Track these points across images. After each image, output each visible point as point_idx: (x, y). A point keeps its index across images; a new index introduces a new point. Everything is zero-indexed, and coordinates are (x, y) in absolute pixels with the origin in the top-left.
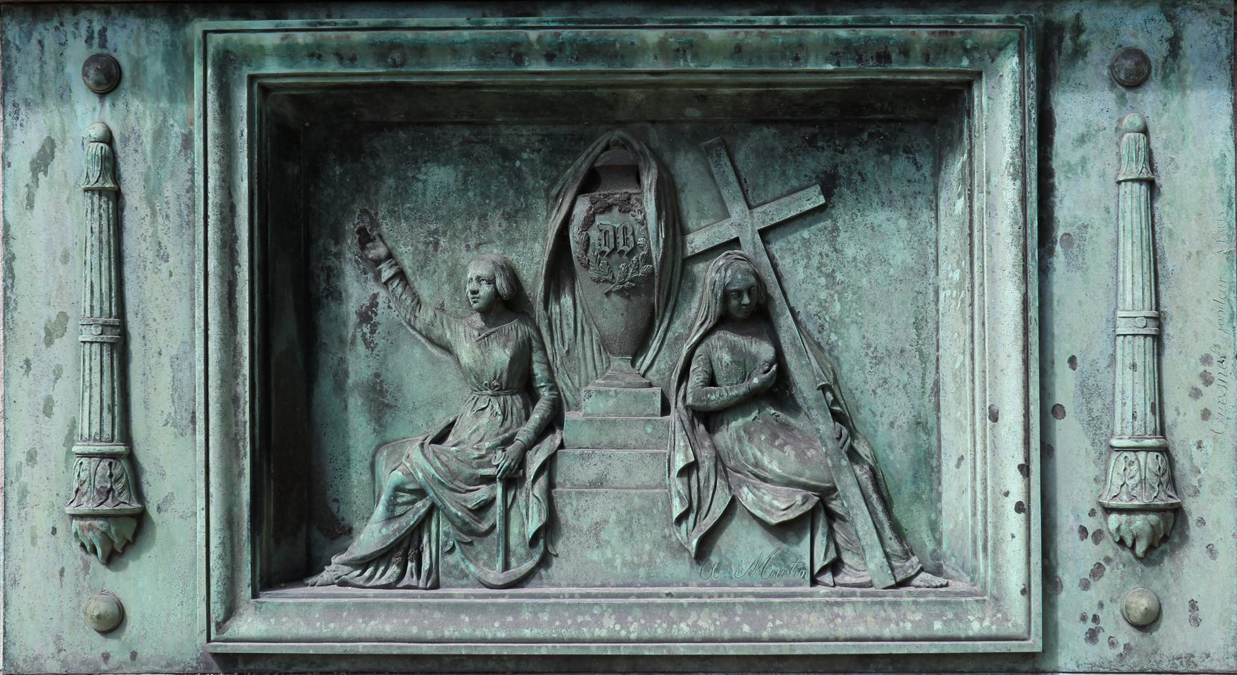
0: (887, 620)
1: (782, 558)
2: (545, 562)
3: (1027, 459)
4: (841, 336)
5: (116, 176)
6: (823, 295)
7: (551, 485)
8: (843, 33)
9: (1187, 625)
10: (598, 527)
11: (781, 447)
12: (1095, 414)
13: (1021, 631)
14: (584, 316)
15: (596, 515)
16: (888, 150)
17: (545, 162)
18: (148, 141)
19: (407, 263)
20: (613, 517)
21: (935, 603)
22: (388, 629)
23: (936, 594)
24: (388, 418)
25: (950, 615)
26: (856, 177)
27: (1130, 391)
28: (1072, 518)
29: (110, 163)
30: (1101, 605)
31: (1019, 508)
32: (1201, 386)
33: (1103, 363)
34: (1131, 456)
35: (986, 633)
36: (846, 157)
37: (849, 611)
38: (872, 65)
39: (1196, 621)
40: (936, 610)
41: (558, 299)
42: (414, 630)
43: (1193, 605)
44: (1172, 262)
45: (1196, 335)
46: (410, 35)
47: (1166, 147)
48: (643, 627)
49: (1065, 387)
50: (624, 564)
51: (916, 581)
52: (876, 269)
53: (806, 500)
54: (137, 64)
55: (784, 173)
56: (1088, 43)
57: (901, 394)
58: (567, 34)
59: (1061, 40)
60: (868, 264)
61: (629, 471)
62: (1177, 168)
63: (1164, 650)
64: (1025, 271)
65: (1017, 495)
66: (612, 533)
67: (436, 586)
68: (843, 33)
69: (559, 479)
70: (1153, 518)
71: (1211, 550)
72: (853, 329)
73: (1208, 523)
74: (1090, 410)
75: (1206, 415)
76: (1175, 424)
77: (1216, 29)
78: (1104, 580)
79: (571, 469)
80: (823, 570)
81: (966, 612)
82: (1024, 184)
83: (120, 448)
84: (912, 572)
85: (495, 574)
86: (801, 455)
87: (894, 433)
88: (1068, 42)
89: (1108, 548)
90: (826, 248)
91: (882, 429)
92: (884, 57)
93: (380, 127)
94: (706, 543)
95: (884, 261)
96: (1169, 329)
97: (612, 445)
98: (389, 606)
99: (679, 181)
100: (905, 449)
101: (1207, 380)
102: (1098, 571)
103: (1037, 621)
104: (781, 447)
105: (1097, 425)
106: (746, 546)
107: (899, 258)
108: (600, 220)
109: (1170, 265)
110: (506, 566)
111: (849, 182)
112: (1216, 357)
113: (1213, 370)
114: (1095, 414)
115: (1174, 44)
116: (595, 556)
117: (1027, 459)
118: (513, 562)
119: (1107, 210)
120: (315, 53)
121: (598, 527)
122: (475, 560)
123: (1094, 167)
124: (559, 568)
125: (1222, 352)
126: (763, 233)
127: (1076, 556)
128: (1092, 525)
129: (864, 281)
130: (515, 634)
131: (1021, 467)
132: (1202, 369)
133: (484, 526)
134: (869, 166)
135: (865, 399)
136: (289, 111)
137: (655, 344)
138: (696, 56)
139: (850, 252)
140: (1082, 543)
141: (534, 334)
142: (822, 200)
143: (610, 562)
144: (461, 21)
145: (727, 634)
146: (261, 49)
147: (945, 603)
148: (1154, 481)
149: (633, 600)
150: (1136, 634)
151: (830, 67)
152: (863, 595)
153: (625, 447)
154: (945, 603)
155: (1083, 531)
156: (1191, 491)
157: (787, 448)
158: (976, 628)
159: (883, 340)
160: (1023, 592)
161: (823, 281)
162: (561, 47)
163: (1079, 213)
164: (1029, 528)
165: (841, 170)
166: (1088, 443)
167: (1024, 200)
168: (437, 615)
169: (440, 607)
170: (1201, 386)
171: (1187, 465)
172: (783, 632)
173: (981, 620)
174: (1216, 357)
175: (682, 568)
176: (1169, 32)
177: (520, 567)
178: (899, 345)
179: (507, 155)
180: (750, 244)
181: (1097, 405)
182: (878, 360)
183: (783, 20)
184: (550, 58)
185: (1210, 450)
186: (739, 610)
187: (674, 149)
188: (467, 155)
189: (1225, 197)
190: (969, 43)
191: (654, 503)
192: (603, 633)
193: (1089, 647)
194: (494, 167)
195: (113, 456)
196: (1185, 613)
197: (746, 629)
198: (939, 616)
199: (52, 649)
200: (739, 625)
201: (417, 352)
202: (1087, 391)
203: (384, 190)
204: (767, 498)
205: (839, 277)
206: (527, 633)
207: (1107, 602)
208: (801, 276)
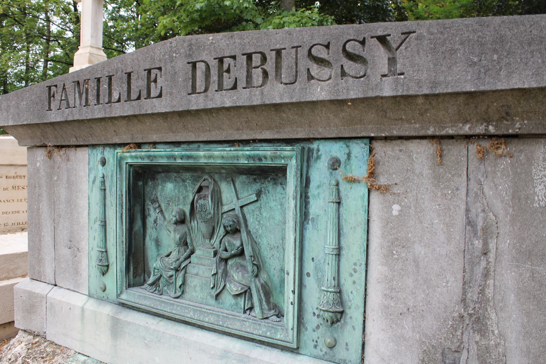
0: (256, 329)
1: (237, 304)
2: (183, 293)
3: (294, 289)
4: (261, 240)
5: (105, 186)
6: (257, 227)
7: (186, 272)
8: (248, 153)
9: (344, 350)
10: (195, 286)
11: (238, 273)
12: (319, 277)
13: (291, 340)
14: (198, 227)
15: (195, 283)
16: (275, 184)
17: (192, 183)
18: (110, 177)
19: (163, 208)
20: (198, 285)
21: (270, 327)
22: (148, 304)
23: (272, 324)
24: (159, 248)
25: (273, 331)
26: (267, 192)
27: (329, 272)
28: (311, 309)
29: (103, 182)
30: (318, 338)
31: (292, 303)
32: (353, 273)
33: (322, 261)
34: (326, 293)
35: (281, 339)
36: (264, 185)
37: (247, 324)
38: (257, 162)
39: (347, 349)
40: (270, 329)
41: (194, 221)
42: (152, 305)
43: (347, 344)
44: (346, 229)
45: (352, 255)
46: (152, 153)
47: (345, 191)
48: (198, 316)
49: (309, 267)
50: (201, 298)
51: (270, 318)
52: (271, 220)
53: (242, 289)
54: (108, 159)
55: (248, 189)
56: (321, 155)
57: (277, 260)
58: (183, 153)
59: (313, 154)
60: (269, 219)
61: (203, 272)
62: (348, 198)
63: (337, 356)
64: (296, 229)
65: (291, 300)
66: (198, 289)
67: (161, 294)
68: (248, 153)
69: (188, 271)
70: (331, 314)
71: (354, 328)
72: (265, 238)
73: (353, 318)
74: (318, 276)
75: (354, 282)
76: (344, 284)
77: (363, 150)
78: (320, 330)
79: (190, 269)
80: (247, 310)
81: (278, 331)
82: (296, 202)
83: (104, 250)
84: (269, 316)
85: (173, 295)
86: (243, 275)
87: (275, 271)
88: (315, 154)
89: (320, 321)
90: (258, 213)
91: (272, 270)
92: (260, 159)
93: (159, 173)
94: (217, 296)
95: (274, 218)
96: (343, 252)
97: (201, 264)
98: (149, 298)
99: (222, 190)
100: (278, 277)
101: (355, 271)
102: (318, 327)
103: (295, 339)
104: (238, 273)
105: (319, 281)
106: (227, 299)
107: (278, 218)
108: (199, 201)
109: (345, 231)
110: (175, 293)
111: (265, 193)
112: (358, 264)
113: (357, 268)
114: (319, 277)
115: (349, 155)
116: (194, 294)
117: (294, 289)
118: (177, 292)
119: (325, 211)
120: (136, 157)
121: (195, 286)
122: (170, 290)
123: (322, 196)
124: (186, 295)
125: (361, 262)
126: (242, 207)
127: (311, 321)
128: (317, 312)
129: (268, 224)
130: (171, 311)
131: (292, 291)
132: (354, 267)
133: (171, 282)
134: (270, 188)
135: (268, 260)
136: (137, 169)
137: (215, 237)
138: (213, 158)
139: (264, 214)
140: (313, 317)
141: (187, 231)
142: (256, 199)
143: (197, 296)
144: (162, 150)
145: (216, 323)
146: (126, 156)
147: (273, 327)
148: (331, 303)
149: (198, 308)
150: (329, 350)
151: (246, 162)
152: (253, 320)
153: (204, 265)
154: (273, 327)
155: (314, 314)
156: (348, 307)
157: (240, 273)
158: (278, 337)
159: (273, 243)
160: (292, 329)
161: (257, 223)
162: (183, 156)
163: (317, 211)
164: (294, 310)
165: (263, 189)
166: (317, 286)
167: (296, 206)
168: (158, 302)
169: (159, 300)
170: (353, 273)
171: (347, 298)
172: (229, 326)
173: (281, 335)
174: (358, 264)
175: (213, 302)
176: (347, 152)
177: (179, 294)
178: (277, 245)
179: (184, 181)
180: (238, 211)
181: (320, 274)
182: (271, 249)
183: (232, 149)
184: (182, 159)
185: (355, 295)
186: (221, 317)
187: (221, 181)
188: (176, 181)
189: (364, 209)
190: (282, 156)
191: (208, 282)
192: (189, 316)
193: (314, 349)
194: (181, 184)
195: (103, 252)
196: (344, 346)
197: (221, 323)
198: (270, 331)
199: (95, 293)
200: (219, 321)
201: (165, 232)
202: (317, 269)
203: (159, 189)
204: (232, 287)
205: (261, 222)
206: (174, 312)
207: (320, 337)
208: (252, 221)
